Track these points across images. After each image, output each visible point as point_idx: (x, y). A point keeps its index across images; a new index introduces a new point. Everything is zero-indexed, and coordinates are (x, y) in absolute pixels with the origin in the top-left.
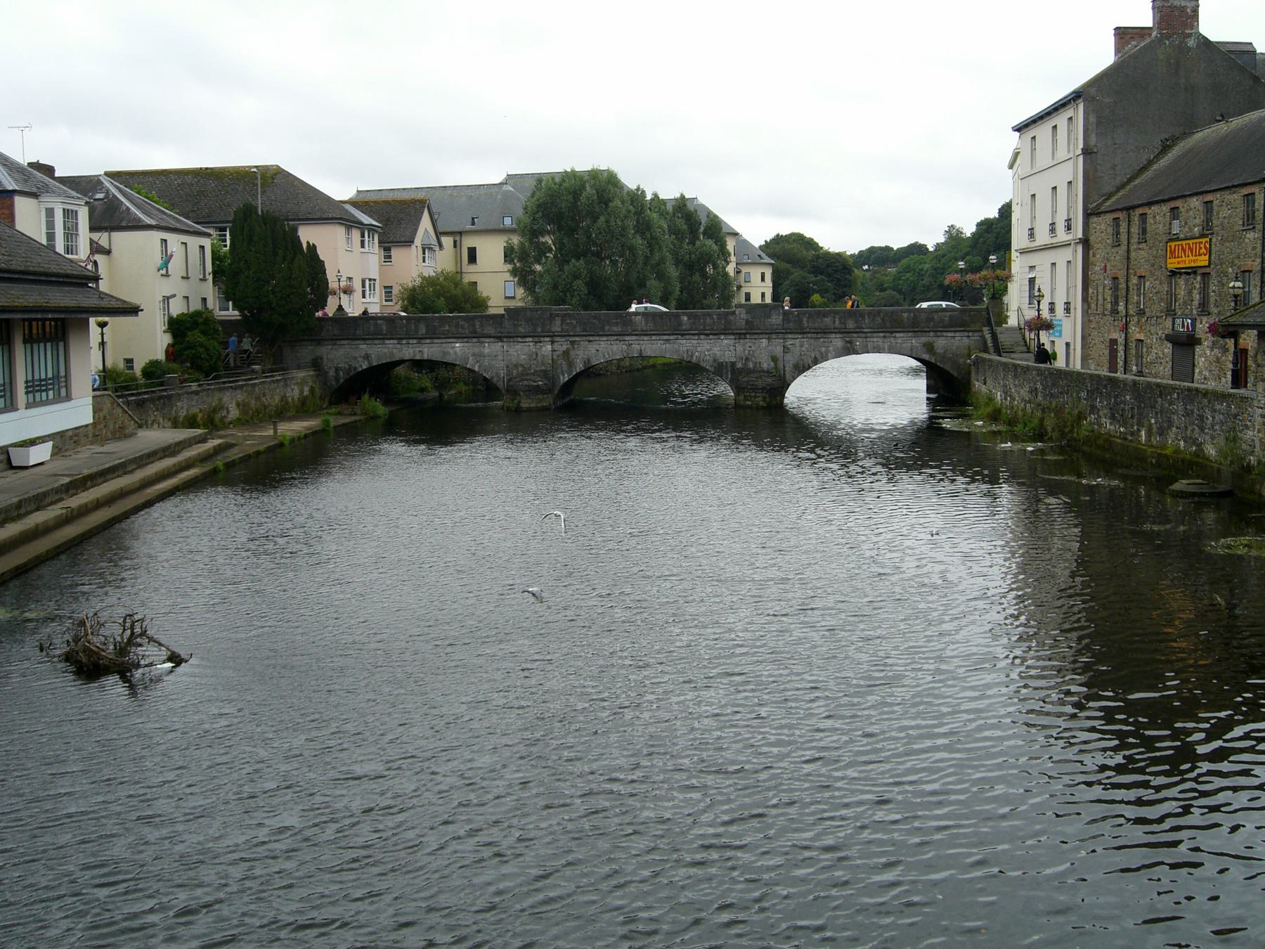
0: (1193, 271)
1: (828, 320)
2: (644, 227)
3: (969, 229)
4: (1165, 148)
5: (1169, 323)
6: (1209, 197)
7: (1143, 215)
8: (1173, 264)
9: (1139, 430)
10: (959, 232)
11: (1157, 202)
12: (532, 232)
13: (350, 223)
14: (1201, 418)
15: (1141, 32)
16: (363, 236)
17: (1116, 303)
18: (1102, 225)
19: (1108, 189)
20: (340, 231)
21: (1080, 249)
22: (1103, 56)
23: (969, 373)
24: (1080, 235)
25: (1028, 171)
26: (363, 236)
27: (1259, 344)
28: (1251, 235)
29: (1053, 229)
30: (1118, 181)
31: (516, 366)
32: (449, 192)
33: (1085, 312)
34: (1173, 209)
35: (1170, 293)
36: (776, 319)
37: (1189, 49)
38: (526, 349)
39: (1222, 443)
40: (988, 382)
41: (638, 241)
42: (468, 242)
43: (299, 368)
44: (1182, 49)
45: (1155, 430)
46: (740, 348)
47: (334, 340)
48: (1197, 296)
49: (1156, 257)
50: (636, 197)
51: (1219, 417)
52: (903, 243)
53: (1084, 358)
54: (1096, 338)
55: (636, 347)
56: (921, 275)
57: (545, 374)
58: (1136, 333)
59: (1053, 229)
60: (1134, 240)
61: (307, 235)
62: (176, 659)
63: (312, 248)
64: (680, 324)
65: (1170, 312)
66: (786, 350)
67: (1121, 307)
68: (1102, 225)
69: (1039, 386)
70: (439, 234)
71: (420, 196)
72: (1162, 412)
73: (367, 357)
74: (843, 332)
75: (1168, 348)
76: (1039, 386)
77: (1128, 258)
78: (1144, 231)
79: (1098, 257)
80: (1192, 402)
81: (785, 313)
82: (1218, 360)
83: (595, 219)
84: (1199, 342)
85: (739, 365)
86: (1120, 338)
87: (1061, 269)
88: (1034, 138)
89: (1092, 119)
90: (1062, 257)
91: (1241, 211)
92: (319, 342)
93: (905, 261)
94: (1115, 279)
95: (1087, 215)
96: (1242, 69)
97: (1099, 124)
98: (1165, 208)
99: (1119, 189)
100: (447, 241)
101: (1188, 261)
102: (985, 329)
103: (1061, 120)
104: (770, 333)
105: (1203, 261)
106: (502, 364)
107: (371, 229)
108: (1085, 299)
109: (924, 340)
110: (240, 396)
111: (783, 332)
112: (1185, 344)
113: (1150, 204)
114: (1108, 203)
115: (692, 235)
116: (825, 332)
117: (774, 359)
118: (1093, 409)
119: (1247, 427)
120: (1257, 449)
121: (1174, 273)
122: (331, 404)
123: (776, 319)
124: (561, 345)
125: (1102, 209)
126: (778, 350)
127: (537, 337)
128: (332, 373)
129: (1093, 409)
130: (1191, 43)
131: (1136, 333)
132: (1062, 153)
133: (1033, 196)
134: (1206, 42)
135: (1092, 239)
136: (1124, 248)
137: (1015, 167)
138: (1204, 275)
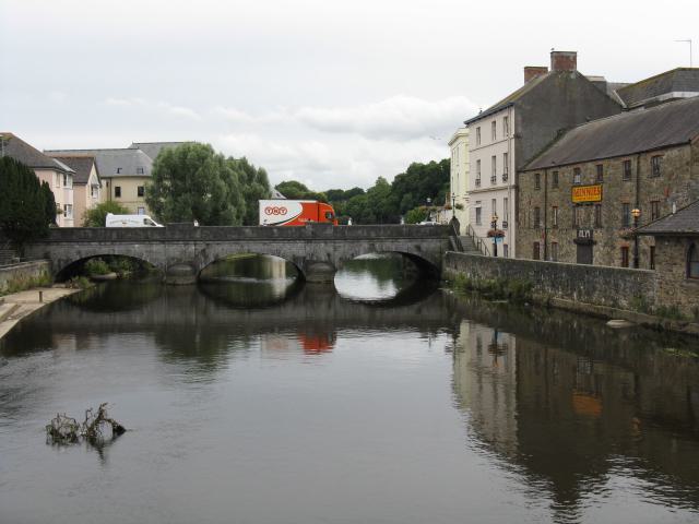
0: (590, 204)
1: (360, 232)
2: (225, 176)
3: (390, 180)
4: (560, 135)
5: (574, 233)
6: (600, 163)
7: (556, 174)
8: (576, 200)
9: (572, 293)
10: (384, 180)
11: (564, 165)
12: (158, 177)
13: (59, 171)
14: (616, 285)
15: (542, 70)
16: (65, 178)
17: (538, 220)
18: (527, 178)
19: (528, 157)
20: (54, 175)
21: (513, 192)
22: (517, 82)
23: (441, 262)
24: (513, 183)
25: (474, 148)
26: (65, 178)
27: (231, 262)
28: (629, 184)
29: (494, 179)
30: (533, 154)
31: (173, 259)
32: (102, 153)
33: (517, 227)
34: (575, 169)
35: (574, 216)
36: (329, 231)
37: (571, 80)
38: (179, 249)
39: (632, 297)
40: (459, 267)
41: (223, 183)
42: (116, 183)
43: (38, 259)
44: (568, 80)
45: (583, 292)
46: (308, 249)
47: (57, 242)
48: (593, 217)
49: (565, 195)
50: (220, 160)
51: (629, 284)
52: (350, 188)
53: (517, 254)
54: (525, 242)
55: (246, 247)
56: (363, 206)
57: (191, 264)
58: (551, 239)
59: (494, 179)
60: (550, 186)
61: (42, 176)
62: (119, 431)
63: (46, 185)
64: (273, 233)
65: (575, 227)
66: (335, 249)
67: (542, 224)
68: (527, 178)
69: (499, 269)
70: (100, 178)
71: (90, 155)
72: (588, 282)
73: (79, 252)
74: (369, 239)
75: (574, 248)
76: (499, 269)
77: (546, 197)
78: (556, 181)
79: (526, 194)
80: (610, 277)
81: (335, 228)
82: (608, 253)
83: (197, 169)
84: (595, 243)
85: (308, 258)
86: (542, 242)
87: (500, 203)
88: (479, 128)
89: (520, 118)
90: (500, 197)
91: (622, 169)
92: (48, 243)
93: (353, 199)
94: (537, 208)
95: (518, 172)
96: (600, 92)
97: (523, 121)
98: (571, 168)
99: (534, 158)
100: (104, 182)
101: (586, 198)
102: (451, 237)
103: (499, 119)
104: (326, 240)
105: (597, 198)
106: (164, 258)
107: (70, 174)
108: (517, 220)
109: (415, 243)
110: (10, 276)
111: (333, 239)
112: (586, 245)
113: (560, 166)
114: (530, 165)
115: (251, 183)
116: (358, 239)
117: (329, 255)
118: (539, 281)
119: (648, 290)
120: (656, 302)
121: (578, 205)
122: (57, 281)
123: (329, 231)
124: (201, 246)
125: (528, 168)
126: (331, 249)
127: (186, 242)
128: (56, 262)
129: (539, 281)
130: (573, 76)
131: (551, 239)
132: (500, 136)
133: (479, 161)
134: (581, 77)
135: (521, 186)
136: (543, 190)
137: (454, 146)
138: (597, 206)
